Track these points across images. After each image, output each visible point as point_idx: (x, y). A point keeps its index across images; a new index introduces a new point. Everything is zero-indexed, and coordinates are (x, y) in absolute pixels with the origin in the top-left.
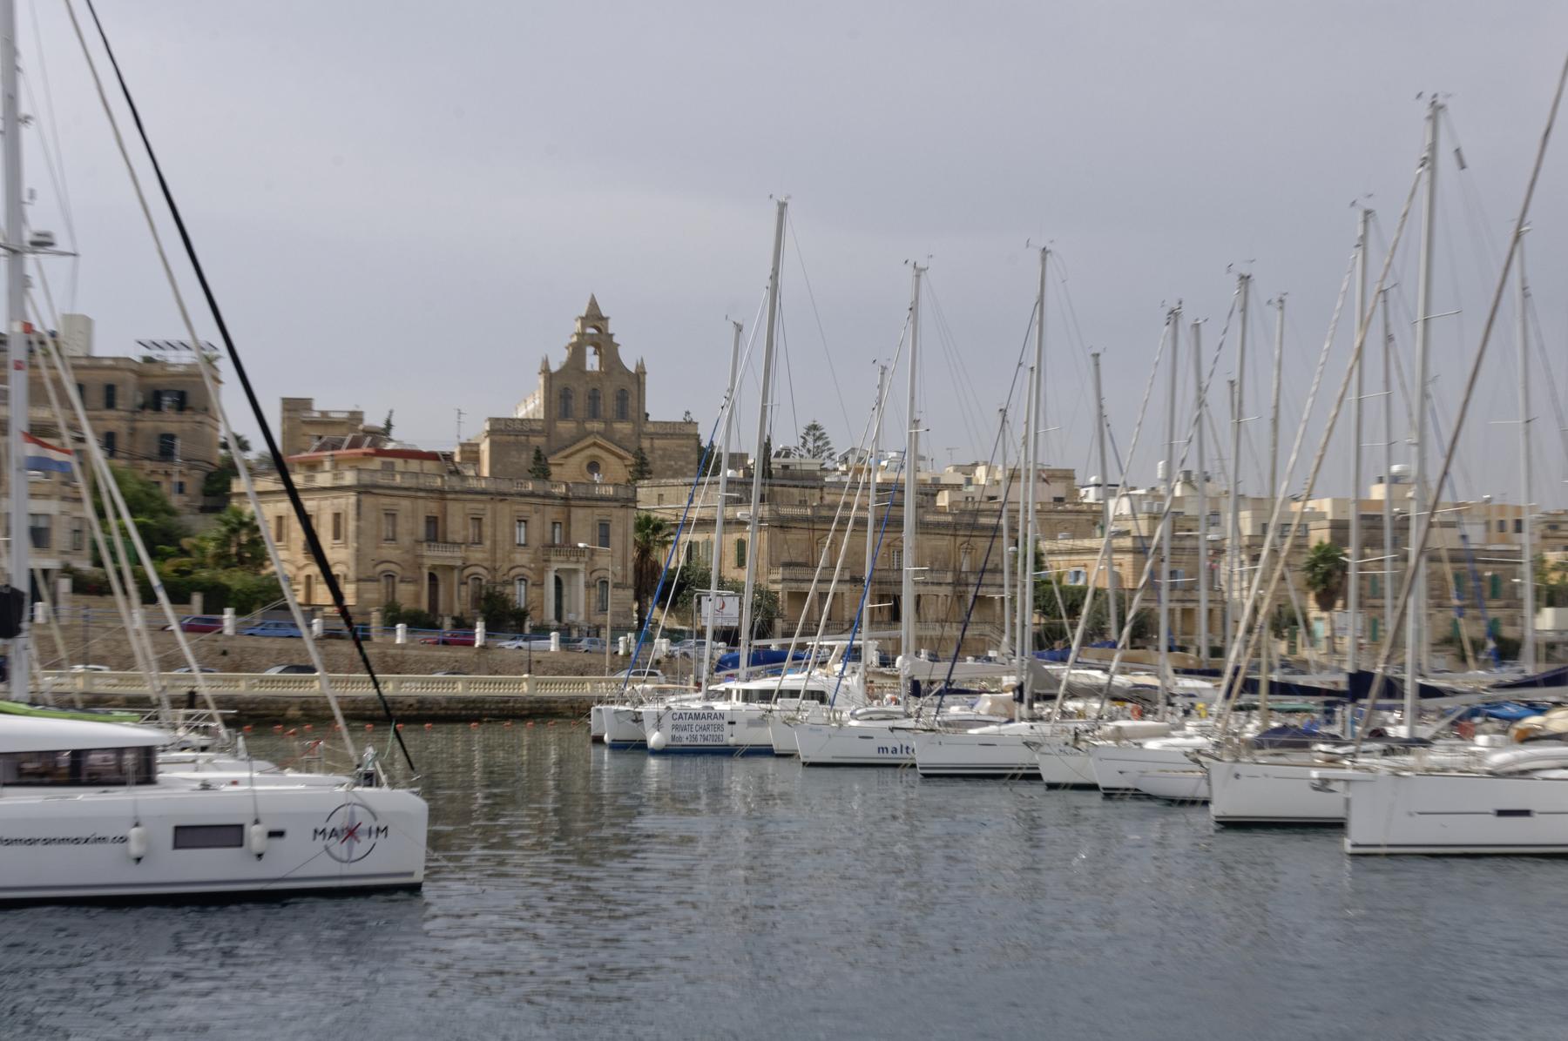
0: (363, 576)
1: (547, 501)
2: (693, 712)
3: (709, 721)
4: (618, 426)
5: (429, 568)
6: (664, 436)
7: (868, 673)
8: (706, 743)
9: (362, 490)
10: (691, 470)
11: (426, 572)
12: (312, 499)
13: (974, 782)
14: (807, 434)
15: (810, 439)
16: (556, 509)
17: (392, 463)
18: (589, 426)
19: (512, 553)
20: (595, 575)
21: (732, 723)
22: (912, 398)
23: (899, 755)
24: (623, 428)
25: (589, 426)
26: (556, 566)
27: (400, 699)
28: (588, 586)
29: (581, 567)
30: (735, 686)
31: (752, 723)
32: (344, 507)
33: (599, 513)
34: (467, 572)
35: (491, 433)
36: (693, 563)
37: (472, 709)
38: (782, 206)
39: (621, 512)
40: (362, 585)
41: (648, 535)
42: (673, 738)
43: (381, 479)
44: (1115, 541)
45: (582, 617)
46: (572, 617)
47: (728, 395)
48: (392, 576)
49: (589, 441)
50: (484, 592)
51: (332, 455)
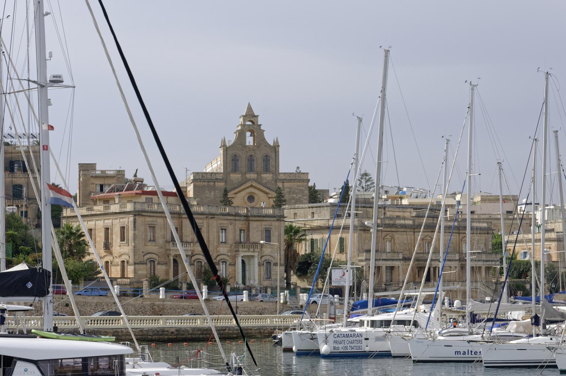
0: (137, 261)
1: (237, 218)
2: (345, 333)
3: (354, 338)
4: (264, 176)
5: (174, 256)
6: (290, 181)
7: (443, 310)
8: (352, 350)
9: (136, 213)
10: (305, 199)
11: (172, 258)
12: (108, 219)
13: (499, 370)
14: (362, 178)
15: (363, 181)
16: (241, 222)
17: (152, 199)
18: (248, 176)
19: (219, 247)
20: (263, 259)
21: (367, 339)
22: (470, 157)
23: (466, 355)
24: (267, 177)
25: (248, 176)
26: (242, 254)
27: (166, 329)
28: (260, 265)
29: (256, 254)
30: (365, 318)
31: (378, 339)
32: (126, 223)
33: (265, 224)
34: (193, 258)
35: (194, 180)
36: (315, 251)
37: (205, 334)
38: (387, 52)
39: (277, 223)
40: (137, 266)
41: (291, 236)
42: (334, 348)
43: (146, 207)
44: (546, 235)
45: (257, 282)
46: (252, 282)
47: (355, 157)
48: (270, 263)
49: (249, 184)
50: (203, 269)
51: (119, 195)
